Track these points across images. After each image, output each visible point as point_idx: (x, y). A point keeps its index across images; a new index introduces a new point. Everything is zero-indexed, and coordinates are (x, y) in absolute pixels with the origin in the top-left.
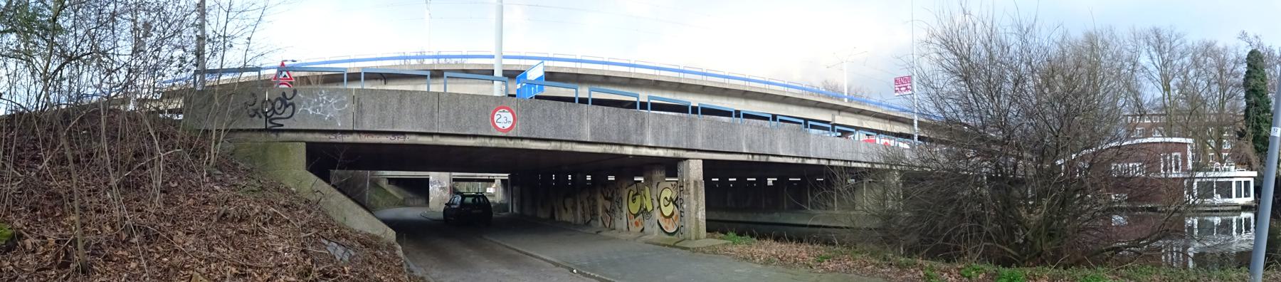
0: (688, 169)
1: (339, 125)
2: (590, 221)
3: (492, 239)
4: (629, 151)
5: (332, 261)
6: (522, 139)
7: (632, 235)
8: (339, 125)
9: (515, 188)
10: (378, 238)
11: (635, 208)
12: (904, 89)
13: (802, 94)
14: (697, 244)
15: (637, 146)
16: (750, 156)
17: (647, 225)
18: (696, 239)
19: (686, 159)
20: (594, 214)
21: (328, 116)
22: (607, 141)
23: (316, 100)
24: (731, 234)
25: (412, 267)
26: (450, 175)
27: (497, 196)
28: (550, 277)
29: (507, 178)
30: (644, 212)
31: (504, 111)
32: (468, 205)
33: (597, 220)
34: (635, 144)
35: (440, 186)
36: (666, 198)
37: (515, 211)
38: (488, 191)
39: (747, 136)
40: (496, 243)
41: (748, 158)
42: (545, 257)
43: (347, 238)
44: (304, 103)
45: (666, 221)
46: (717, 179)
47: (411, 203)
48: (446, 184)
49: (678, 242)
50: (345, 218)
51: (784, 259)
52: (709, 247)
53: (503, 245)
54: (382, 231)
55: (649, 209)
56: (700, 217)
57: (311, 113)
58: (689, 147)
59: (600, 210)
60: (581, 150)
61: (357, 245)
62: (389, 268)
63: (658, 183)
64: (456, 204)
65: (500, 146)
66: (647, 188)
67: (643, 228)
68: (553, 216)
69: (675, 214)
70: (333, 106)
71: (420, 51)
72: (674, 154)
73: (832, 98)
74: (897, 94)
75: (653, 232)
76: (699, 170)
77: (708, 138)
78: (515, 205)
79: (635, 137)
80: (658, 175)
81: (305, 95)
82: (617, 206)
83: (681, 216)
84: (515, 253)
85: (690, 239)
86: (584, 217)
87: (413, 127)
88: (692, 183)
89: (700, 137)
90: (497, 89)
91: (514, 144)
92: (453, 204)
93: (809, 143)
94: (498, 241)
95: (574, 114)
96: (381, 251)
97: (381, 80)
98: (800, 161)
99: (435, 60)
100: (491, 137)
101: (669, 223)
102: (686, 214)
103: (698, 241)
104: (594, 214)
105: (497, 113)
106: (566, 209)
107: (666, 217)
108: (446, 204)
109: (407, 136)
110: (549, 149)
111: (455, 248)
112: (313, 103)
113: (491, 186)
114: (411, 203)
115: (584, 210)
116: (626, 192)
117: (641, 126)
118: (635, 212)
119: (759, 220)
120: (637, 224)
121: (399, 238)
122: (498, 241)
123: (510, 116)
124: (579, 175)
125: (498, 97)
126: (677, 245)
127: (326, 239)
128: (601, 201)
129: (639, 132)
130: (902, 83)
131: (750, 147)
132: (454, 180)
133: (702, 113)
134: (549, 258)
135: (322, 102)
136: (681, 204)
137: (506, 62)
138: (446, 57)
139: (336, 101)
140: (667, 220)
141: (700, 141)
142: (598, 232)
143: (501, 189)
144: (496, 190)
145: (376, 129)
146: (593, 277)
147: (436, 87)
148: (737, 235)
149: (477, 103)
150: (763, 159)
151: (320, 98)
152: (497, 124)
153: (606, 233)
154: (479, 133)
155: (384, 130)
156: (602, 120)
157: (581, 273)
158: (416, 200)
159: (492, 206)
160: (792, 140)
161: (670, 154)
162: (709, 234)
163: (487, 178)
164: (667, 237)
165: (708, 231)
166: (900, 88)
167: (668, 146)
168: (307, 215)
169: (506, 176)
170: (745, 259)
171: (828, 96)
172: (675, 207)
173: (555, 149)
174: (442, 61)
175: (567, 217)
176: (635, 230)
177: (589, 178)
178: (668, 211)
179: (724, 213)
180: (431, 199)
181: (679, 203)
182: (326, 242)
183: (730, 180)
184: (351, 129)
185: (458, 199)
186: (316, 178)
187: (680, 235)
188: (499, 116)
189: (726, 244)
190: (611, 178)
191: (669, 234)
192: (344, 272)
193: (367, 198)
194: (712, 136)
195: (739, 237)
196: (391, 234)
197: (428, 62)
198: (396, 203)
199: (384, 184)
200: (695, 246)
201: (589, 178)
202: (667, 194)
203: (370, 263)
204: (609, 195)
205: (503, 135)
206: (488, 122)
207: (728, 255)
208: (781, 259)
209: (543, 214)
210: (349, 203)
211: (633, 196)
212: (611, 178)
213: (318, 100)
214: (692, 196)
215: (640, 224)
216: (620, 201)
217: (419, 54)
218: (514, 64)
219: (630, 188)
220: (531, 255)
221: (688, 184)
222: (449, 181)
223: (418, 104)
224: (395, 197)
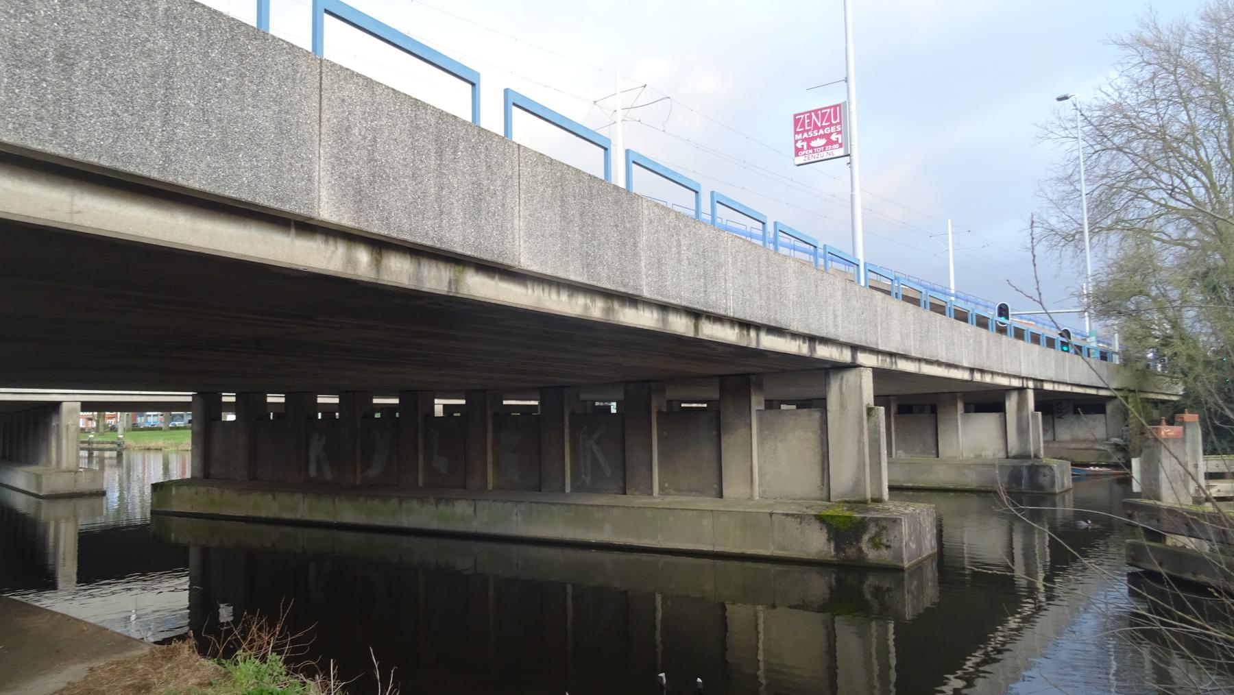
12: (822, 142)
16: (363, 256)
39: (343, 131)
41: (351, 262)
71: (1026, 682)
74: (800, 160)
93: (634, 232)
98: (595, 310)
119: (406, 521)
130: (816, 127)
131: (359, 197)
150: (435, 279)
160: (573, 212)
166: (809, 140)
183: (376, 401)
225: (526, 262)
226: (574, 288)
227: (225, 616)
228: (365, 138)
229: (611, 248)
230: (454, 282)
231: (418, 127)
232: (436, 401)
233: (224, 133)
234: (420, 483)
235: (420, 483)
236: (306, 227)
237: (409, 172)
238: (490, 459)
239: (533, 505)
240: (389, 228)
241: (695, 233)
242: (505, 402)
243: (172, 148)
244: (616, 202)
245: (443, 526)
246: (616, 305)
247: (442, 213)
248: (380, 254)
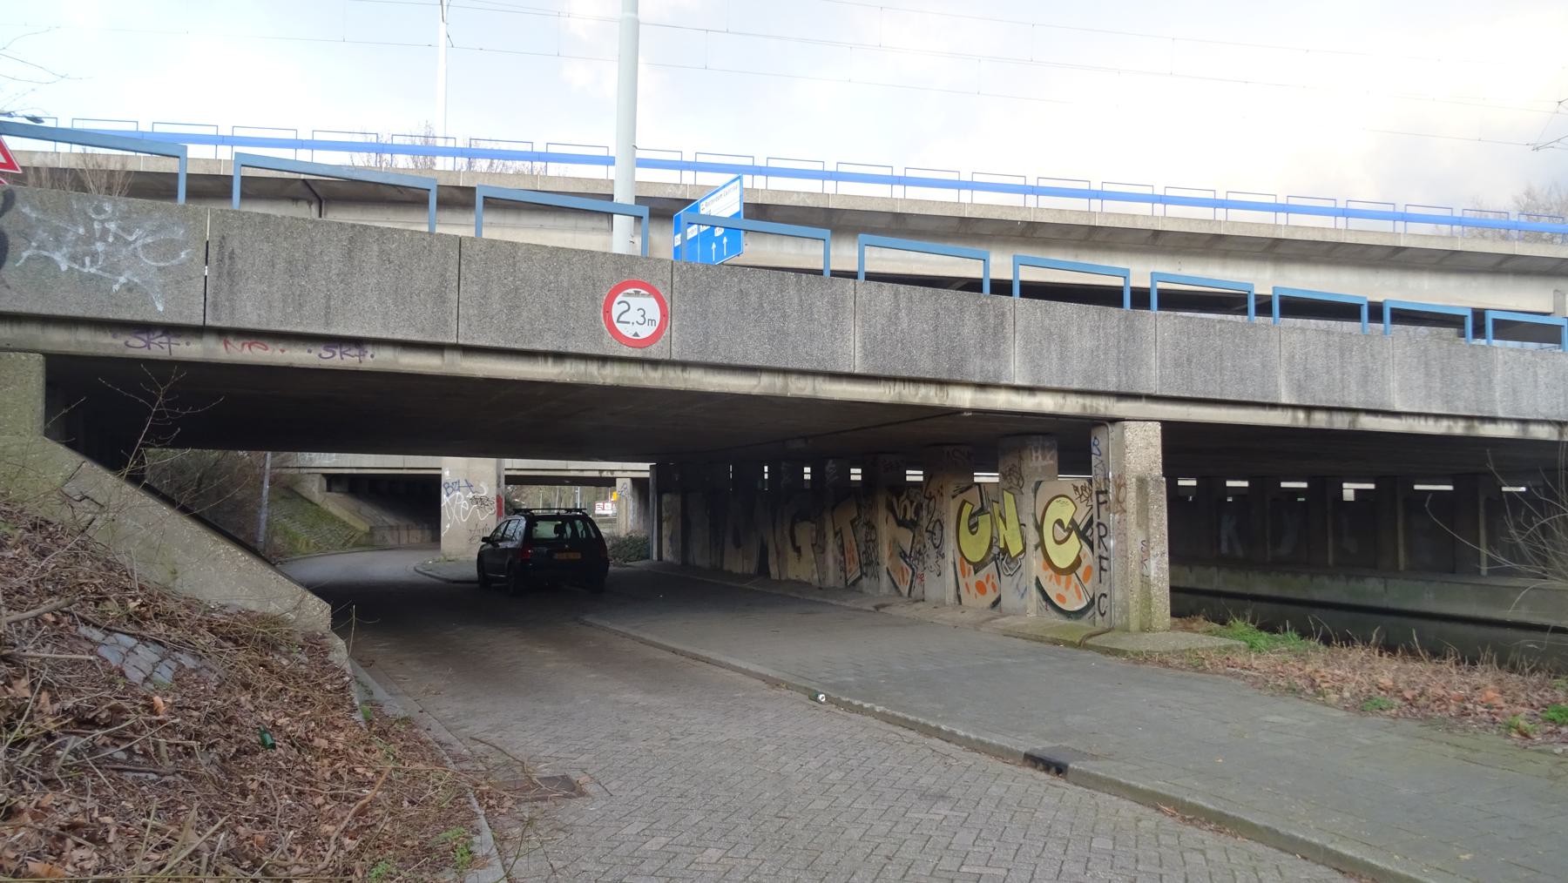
0: (1122, 446)
1: (160, 308)
2: (860, 578)
3: (607, 624)
4: (964, 398)
5: (111, 684)
6: (684, 365)
7: (969, 616)
8: (160, 308)
9: (666, 498)
10: (276, 621)
11: (975, 548)
13: (1452, 237)
14: (1146, 643)
15: (982, 386)
16: (1301, 415)
17: (1007, 587)
18: (1143, 629)
19: (1114, 421)
20: (869, 563)
21: (122, 280)
22: (905, 374)
23: (81, 231)
24: (1239, 625)
25: (380, 694)
26: (498, 467)
27: (622, 520)
28: (758, 710)
29: (647, 475)
30: (1000, 556)
31: (637, 293)
32: (545, 542)
33: (877, 577)
34: (977, 380)
35: (471, 495)
36: (1060, 522)
37: (667, 556)
38: (598, 511)
40: (616, 633)
41: (1295, 419)
42: (744, 666)
43: (172, 622)
44: (42, 234)
45: (1058, 582)
46: (1193, 483)
47: (391, 541)
48: (488, 489)
49: (1091, 636)
50: (175, 572)
51: (1422, 701)
52: (1180, 654)
53: (634, 638)
54: (289, 603)
55: (1015, 548)
56: (1153, 574)
57: (64, 267)
58: (1123, 389)
59: (885, 552)
60: (837, 397)
61: (206, 640)
62: (305, 698)
63: (1039, 483)
64: (511, 539)
65: (626, 383)
66: (1008, 497)
67: (999, 600)
68: (763, 569)
69: (1085, 563)
70: (141, 254)
72: (1084, 407)
73: (1551, 240)
75: (1025, 608)
76: (1152, 450)
77: (1177, 364)
78: (666, 542)
79: (978, 362)
80: (1039, 461)
81: (45, 211)
82: (929, 545)
83: (1101, 569)
84: (667, 656)
85: (1126, 629)
86: (844, 570)
87: (385, 326)
88: (1132, 484)
89: (1153, 362)
90: (621, 237)
91: (662, 378)
92: (503, 539)
94: (623, 629)
95: (821, 305)
96: (287, 655)
97: (310, 203)
98: (1459, 429)
99: (462, 163)
100: (604, 359)
101: (1067, 588)
102: (1115, 565)
103: (1147, 635)
104: (869, 564)
105: (620, 298)
106: (798, 550)
107: (1059, 571)
108: (484, 539)
109: (370, 350)
110: (756, 391)
111: (506, 646)
112: (70, 237)
113: (606, 499)
114: (391, 541)
115: (843, 554)
116: (953, 506)
117: (995, 335)
118: (976, 555)
119: (1318, 595)
120: (981, 588)
121: (339, 623)
122: (623, 629)
123: (652, 307)
124: (830, 466)
125: (620, 256)
126: (1090, 642)
127: (96, 626)
128: (886, 530)
129: (988, 350)
131: (1299, 388)
132: (510, 480)
133: (1162, 306)
134: (753, 668)
135: (103, 238)
136: (1101, 537)
137: (644, 175)
138: (492, 155)
139: (149, 240)
140: (1063, 578)
141: (1155, 373)
142: (877, 608)
143: (631, 505)
144: (618, 508)
145: (275, 326)
146: (871, 712)
147: (456, 226)
148: (1261, 628)
149: (566, 269)
150: (1341, 422)
151: (96, 226)
152: (618, 326)
153: (901, 610)
154: (571, 349)
155: (300, 329)
156: (893, 319)
157: (838, 703)
158: (404, 533)
159: (608, 545)
161: (1073, 406)
162: (1176, 620)
163: (596, 474)
164: (1063, 621)
165: (1175, 614)
167: (1066, 386)
168: (33, 562)
169: (643, 469)
170: (1293, 690)
171: (1536, 236)
172: (1086, 548)
173: (770, 392)
174: (482, 165)
175: (800, 569)
176: (977, 602)
177: (856, 474)
178: (1064, 555)
179: (1214, 570)
180: (446, 527)
181: (1094, 534)
182: (97, 635)
183: (1230, 484)
184: (197, 321)
185: (518, 526)
186: (80, 459)
187: (1098, 618)
188: (625, 307)
189: (1228, 648)
190: (914, 476)
191: (1068, 614)
192: (151, 709)
193: (263, 526)
194: (1189, 361)
195: (1265, 634)
196: (318, 612)
197: (443, 164)
198: (348, 541)
199: (315, 489)
200: (1142, 648)
201: (856, 474)
202: (1063, 511)
203: (246, 686)
204: (910, 515)
205: (633, 355)
206: (596, 319)
207: (1237, 676)
208: (1411, 703)
209: (738, 564)
210: (188, 530)
211: (972, 516)
212: (914, 476)
213: (90, 230)
214: (1132, 518)
215: (989, 588)
216: (937, 532)
217: (418, 142)
218: (666, 182)
219: (960, 498)
220: (708, 661)
221: (1121, 486)
222: (494, 482)
223: (401, 266)
224: (345, 525)
225: (1399, 407)
226: (1438, 417)
227: (1499, 351)
228: (1301, 359)
229: (1467, 388)
230: (1353, 422)
231: (1329, 345)
232: (1345, 485)
233: (1241, 373)
234: (1330, 561)
235: (1330, 561)
236: (1274, 406)
237: (1325, 370)
238: (1401, 541)
239: (1446, 585)
240: (1315, 401)
241: (1553, 364)
242: (1417, 487)
243: (1222, 385)
244: (1472, 356)
245: (1354, 601)
246: (1476, 423)
247: (1344, 388)
248: (1309, 413)
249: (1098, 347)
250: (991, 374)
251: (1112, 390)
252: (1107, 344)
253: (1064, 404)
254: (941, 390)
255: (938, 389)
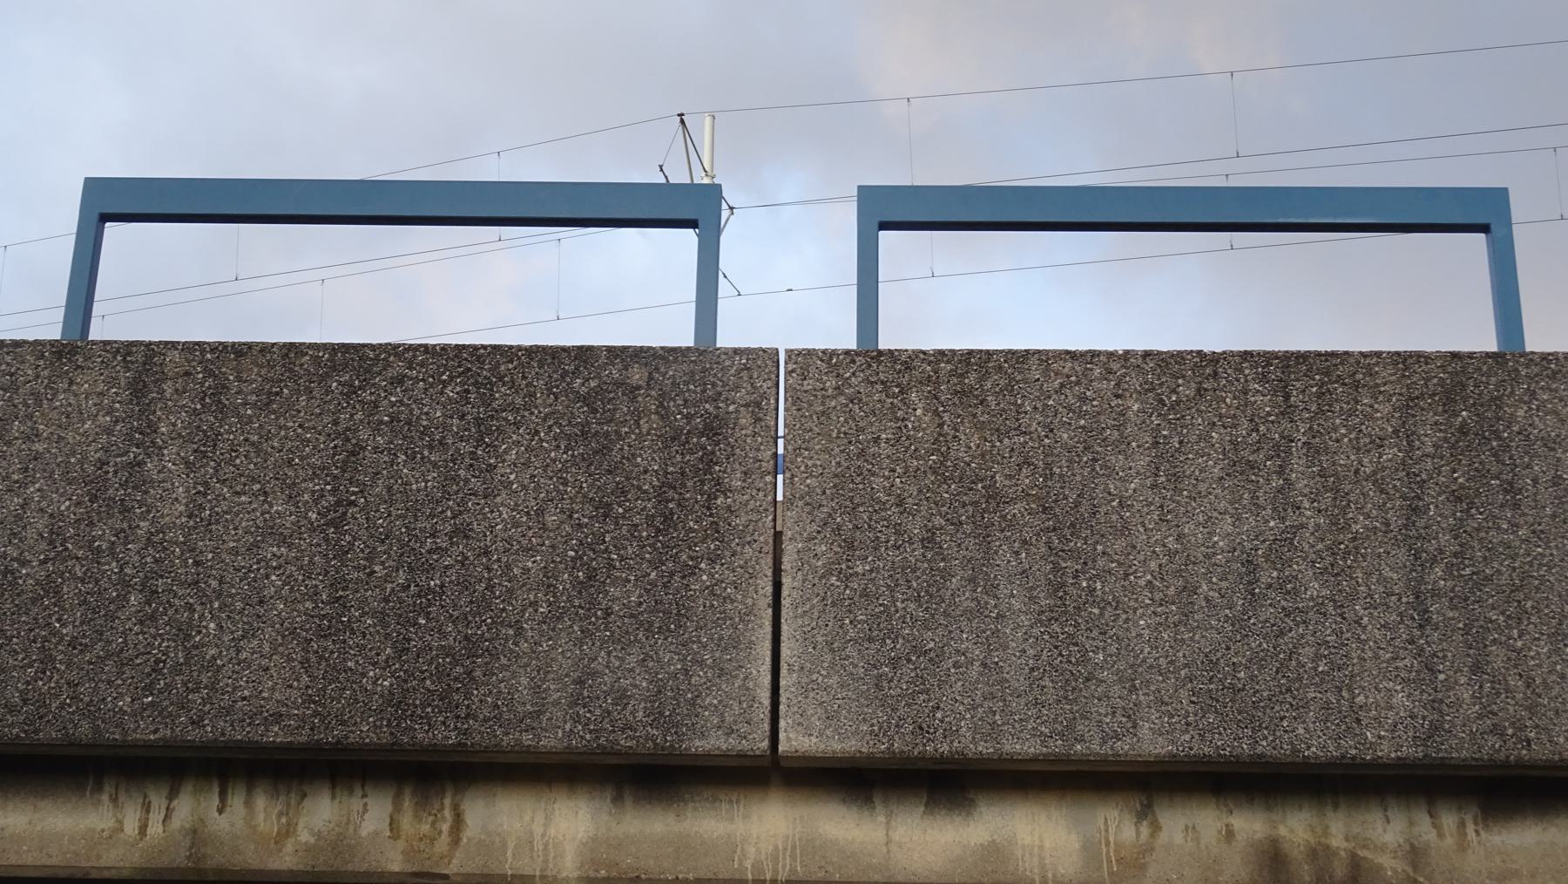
129: (624, 595)
167: (1090, 745)
249: (1287, 539)
250: (639, 712)
251: (1386, 751)
252: (1339, 524)
253: (1149, 849)
254: (422, 804)
255: (407, 803)
